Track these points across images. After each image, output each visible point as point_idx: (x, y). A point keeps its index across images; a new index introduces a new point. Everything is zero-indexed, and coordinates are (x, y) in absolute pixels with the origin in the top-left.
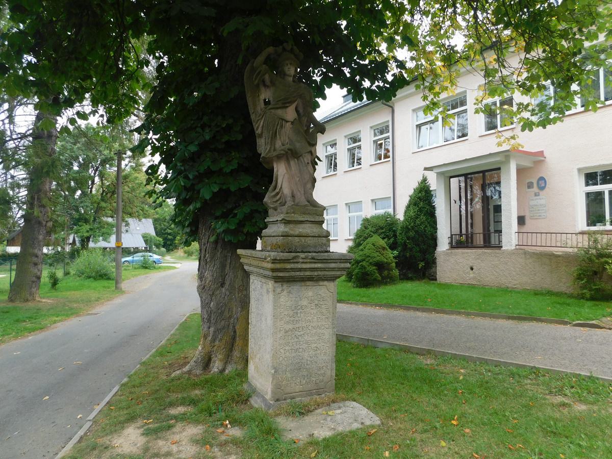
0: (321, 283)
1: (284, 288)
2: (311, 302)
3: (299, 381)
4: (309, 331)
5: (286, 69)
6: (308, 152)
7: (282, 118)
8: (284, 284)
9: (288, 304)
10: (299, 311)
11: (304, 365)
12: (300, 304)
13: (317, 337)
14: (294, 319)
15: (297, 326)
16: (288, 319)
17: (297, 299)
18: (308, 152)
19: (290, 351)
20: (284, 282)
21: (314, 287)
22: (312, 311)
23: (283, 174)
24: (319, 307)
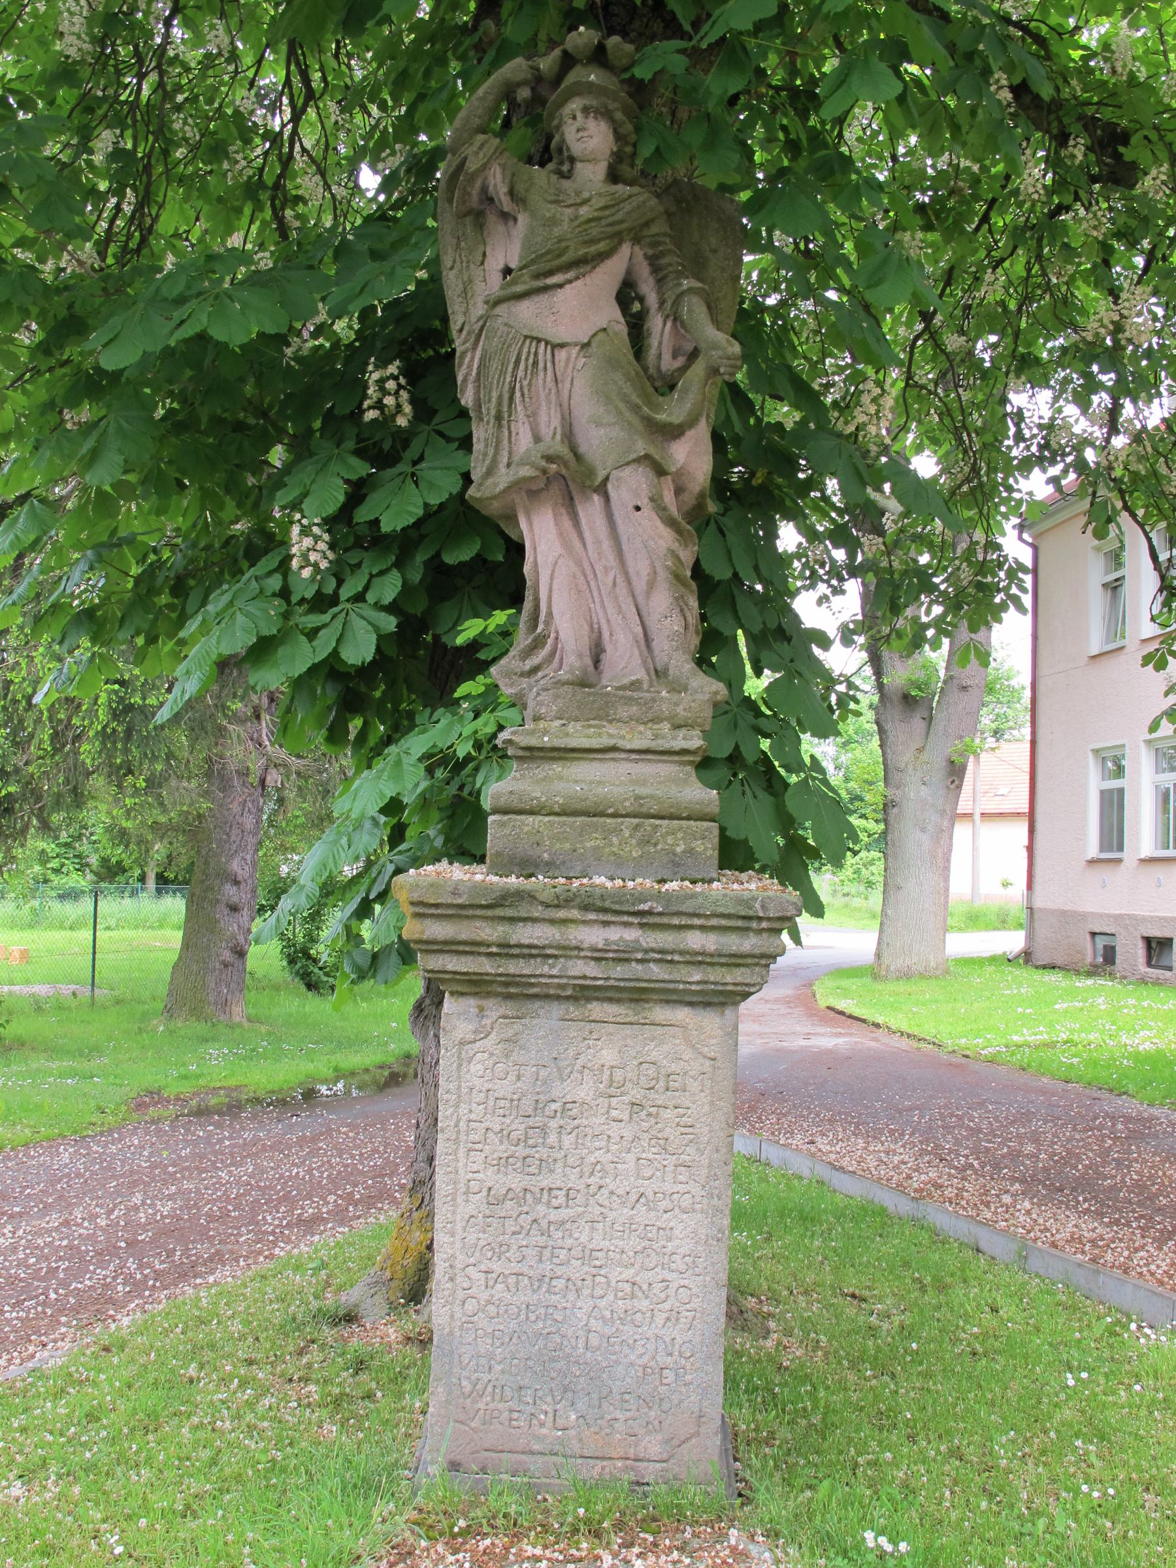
0: (661, 1013)
1: (487, 1022)
2: (613, 1089)
3: (550, 1409)
4: (597, 1210)
5: (570, 133)
6: (638, 460)
7: (534, 334)
8: (490, 1003)
9: (504, 1088)
10: (553, 1124)
11: (575, 1348)
12: (556, 1093)
13: (634, 1243)
14: (528, 1151)
15: (545, 1183)
16: (502, 1149)
17: (543, 1073)
18: (638, 460)
19: (512, 1280)
20: (488, 995)
21: (628, 1030)
22: (615, 1130)
23: (551, 559)
24: (649, 1115)
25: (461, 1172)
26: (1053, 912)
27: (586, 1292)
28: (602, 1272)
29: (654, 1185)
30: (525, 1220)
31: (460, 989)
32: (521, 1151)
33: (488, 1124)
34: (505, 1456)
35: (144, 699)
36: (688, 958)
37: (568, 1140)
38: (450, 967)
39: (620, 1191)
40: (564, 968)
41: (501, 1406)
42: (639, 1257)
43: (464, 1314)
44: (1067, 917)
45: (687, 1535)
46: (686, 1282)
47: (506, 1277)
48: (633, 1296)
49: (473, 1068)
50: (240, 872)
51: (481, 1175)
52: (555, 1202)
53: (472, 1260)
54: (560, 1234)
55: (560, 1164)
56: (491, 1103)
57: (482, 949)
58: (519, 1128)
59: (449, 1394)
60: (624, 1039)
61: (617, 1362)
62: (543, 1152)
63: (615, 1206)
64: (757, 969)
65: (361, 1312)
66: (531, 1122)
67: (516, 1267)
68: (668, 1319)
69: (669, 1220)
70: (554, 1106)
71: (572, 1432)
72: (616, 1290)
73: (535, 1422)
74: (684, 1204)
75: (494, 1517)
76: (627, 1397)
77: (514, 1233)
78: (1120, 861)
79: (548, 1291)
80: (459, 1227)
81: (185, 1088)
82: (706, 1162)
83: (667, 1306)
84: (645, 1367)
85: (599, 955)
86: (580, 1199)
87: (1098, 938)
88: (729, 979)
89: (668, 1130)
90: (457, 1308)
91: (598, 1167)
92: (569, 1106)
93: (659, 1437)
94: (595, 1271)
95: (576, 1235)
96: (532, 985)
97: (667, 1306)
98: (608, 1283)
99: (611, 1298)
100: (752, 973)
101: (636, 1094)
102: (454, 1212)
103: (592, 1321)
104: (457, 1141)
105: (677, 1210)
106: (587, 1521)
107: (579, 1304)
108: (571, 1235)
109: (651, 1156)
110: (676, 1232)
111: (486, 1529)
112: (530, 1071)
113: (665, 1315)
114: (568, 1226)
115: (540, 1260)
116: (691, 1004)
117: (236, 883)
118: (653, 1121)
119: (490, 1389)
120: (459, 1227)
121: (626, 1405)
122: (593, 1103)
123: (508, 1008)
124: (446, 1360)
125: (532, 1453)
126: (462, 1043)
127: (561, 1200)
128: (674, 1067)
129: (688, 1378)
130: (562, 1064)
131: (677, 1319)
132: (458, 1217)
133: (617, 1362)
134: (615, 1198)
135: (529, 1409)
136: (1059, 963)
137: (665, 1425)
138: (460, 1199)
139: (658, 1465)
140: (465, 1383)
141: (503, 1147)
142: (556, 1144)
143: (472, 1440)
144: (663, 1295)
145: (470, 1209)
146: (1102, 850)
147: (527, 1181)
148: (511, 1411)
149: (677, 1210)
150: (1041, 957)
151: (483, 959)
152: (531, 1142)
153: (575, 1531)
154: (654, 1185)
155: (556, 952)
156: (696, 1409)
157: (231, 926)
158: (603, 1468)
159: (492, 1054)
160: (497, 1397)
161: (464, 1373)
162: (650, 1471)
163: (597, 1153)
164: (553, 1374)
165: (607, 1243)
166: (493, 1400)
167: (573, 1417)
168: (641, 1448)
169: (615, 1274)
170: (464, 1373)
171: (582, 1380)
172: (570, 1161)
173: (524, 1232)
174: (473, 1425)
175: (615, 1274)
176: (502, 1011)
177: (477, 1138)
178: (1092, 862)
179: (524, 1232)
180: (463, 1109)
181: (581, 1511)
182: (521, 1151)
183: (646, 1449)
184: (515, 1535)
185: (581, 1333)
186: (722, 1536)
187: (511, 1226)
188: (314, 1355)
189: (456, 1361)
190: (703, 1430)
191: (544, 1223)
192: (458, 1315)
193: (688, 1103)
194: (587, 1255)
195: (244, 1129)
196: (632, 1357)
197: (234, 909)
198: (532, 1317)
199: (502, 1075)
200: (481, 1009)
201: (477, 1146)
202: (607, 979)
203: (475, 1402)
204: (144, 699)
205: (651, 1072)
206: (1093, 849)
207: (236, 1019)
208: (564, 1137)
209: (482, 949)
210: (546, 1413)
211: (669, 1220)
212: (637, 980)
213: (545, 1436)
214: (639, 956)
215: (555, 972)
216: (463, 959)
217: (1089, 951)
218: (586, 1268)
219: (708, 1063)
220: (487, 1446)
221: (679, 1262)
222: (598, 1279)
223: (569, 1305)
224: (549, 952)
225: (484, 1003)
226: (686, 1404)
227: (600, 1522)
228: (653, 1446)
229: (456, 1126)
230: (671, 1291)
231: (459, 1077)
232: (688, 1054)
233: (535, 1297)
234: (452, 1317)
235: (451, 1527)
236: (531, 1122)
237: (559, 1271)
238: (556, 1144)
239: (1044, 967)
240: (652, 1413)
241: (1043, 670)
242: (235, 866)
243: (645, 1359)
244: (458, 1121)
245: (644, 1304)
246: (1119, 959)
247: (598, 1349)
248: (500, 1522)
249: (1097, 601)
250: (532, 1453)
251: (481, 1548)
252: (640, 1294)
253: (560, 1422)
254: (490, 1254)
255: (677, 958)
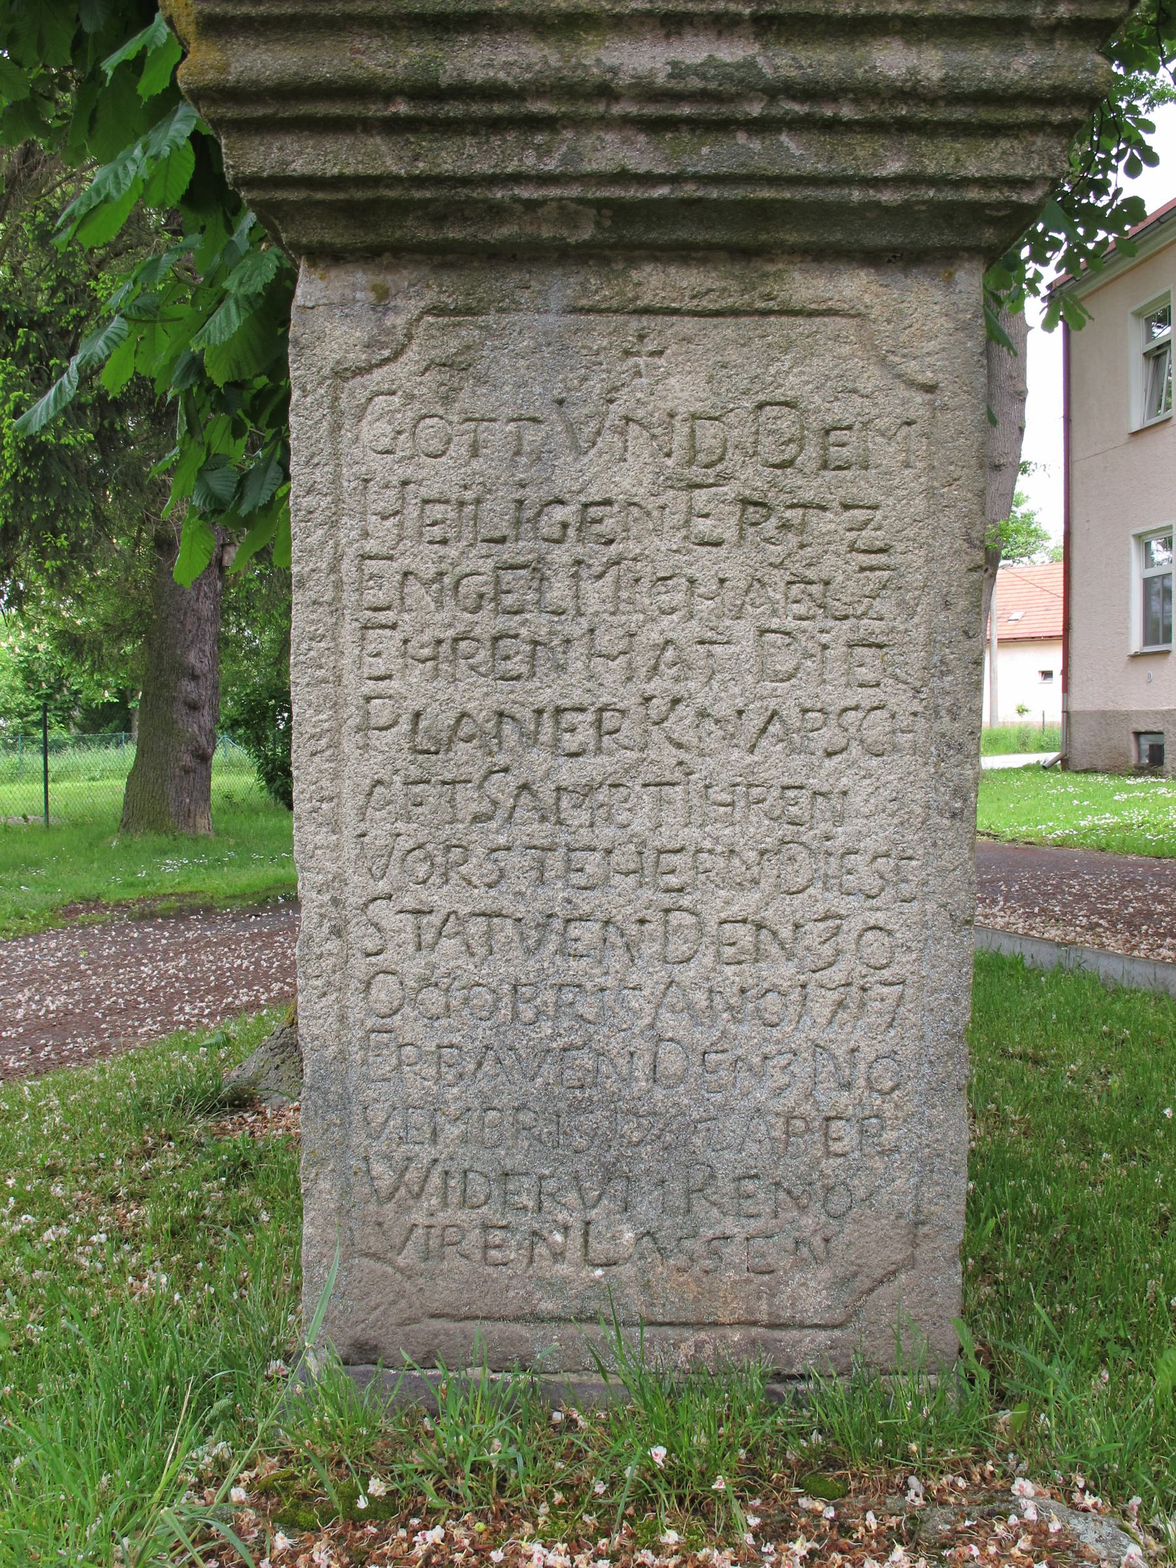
1: (397, 321)
2: (697, 472)
3: (575, 1221)
4: (670, 755)
8: (399, 279)
9: (441, 477)
10: (561, 555)
11: (627, 1080)
12: (563, 483)
13: (758, 829)
15: (546, 697)
16: (445, 620)
17: (532, 436)
21: (728, 328)
22: (705, 565)
24: (785, 526)
25: (349, 679)
26: (1091, 714)
27: (650, 949)
28: (686, 901)
29: (803, 691)
30: (501, 787)
31: (328, 236)
32: (487, 623)
33: (405, 562)
34: (476, 1328)
35: (58, 438)
36: (874, 110)
37: (595, 594)
38: (298, 167)
39: (723, 709)
40: (574, 154)
41: (462, 1216)
42: (770, 868)
43: (370, 1012)
44: (1105, 717)
45: (914, 1497)
46: (880, 918)
47: (462, 921)
48: (758, 955)
49: (367, 431)
50: (198, 665)
51: (394, 685)
52: (570, 742)
53: (383, 886)
54: (585, 817)
55: (579, 649)
56: (412, 512)
57: (374, 110)
58: (480, 564)
59: (346, 1192)
60: (719, 349)
61: (725, 1109)
62: (539, 624)
63: (711, 744)
64: (1039, 142)
65: (260, 1093)
66: (506, 553)
67: (485, 899)
68: (841, 1005)
69: (838, 773)
70: (559, 513)
71: (627, 1271)
72: (719, 943)
73: (541, 1249)
74: (871, 735)
75: (453, 1470)
76: (749, 1186)
77: (476, 819)
78: (1168, 652)
79: (561, 951)
80: (349, 810)
81: (131, 895)
82: (919, 635)
83: (836, 975)
84: (789, 1118)
85: (661, 112)
86: (629, 730)
87: (1143, 739)
88: (972, 169)
89: (830, 560)
90: (354, 1000)
91: (670, 654)
92: (594, 512)
93: (825, 1273)
94: (667, 900)
95: (623, 817)
96: (497, 212)
97: (836, 975)
98: (700, 926)
99: (708, 961)
100: (1028, 154)
101: (751, 478)
102: (336, 776)
103: (665, 1015)
104: (336, 608)
105: (855, 750)
106: (675, 1477)
107: (634, 978)
108: (609, 819)
109: (791, 624)
110: (856, 800)
111: (433, 1500)
112: (500, 433)
113: (835, 996)
114: (601, 796)
115: (541, 881)
116: (873, 259)
117: (194, 677)
118: (793, 539)
119: (435, 1180)
120: (349, 810)
121: (749, 1206)
122: (651, 504)
123: (442, 289)
124: (334, 1117)
125: (537, 1318)
126: (342, 374)
127: (585, 735)
128: (839, 412)
129: (889, 1136)
130: (576, 413)
131: (862, 1005)
132: (347, 787)
133: (725, 1109)
134: (709, 725)
135: (528, 1221)
136: (1100, 765)
137: (838, 1244)
138: (348, 745)
139: (822, 1336)
140: (378, 1168)
141: (444, 616)
142: (569, 604)
143: (401, 1294)
144: (827, 950)
145: (374, 766)
146: (1146, 643)
147: (502, 695)
148: (486, 1227)
149: (855, 750)
150: (1079, 761)
151: (377, 142)
152: (508, 600)
153: (644, 1500)
154: (803, 691)
155: (552, 109)
156: (908, 1208)
157: (192, 727)
158: (699, 1346)
159: (410, 397)
160: (454, 1198)
161: (380, 1146)
162: (805, 1347)
163: (665, 621)
164: (580, 1142)
165: (694, 833)
166: (445, 1204)
167: (629, 1236)
168: (783, 1298)
169: (717, 904)
170: (380, 1146)
171: (645, 1151)
172: (603, 641)
173: (501, 814)
174: (401, 1261)
175: (717, 904)
176: (430, 297)
177: (381, 597)
178: (1136, 656)
179: (501, 814)
180: (349, 528)
181: (659, 1453)
182: (487, 623)
183: (794, 1300)
184: (501, 1514)
185: (640, 1043)
186: (998, 1503)
187: (469, 801)
188: (170, 1156)
189: (357, 1119)
190: (924, 1252)
191: (547, 794)
192: (354, 1015)
193: (873, 495)
194: (651, 861)
195: (189, 930)
196: (761, 1095)
197: (194, 707)
198: (528, 1013)
199: (436, 445)
200: (383, 295)
201: (382, 617)
202: (674, 179)
203: (403, 1209)
204: (58, 438)
205: (787, 423)
206: (1136, 643)
207: (202, 832)
208: (587, 586)
209: (374, 110)
210: (566, 1229)
211: (838, 773)
212: (751, 179)
213: (566, 1281)
214: (755, 110)
215: (551, 165)
216: (330, 144)
217: (1134, 753)
218: (647, 894)
219: (919, 398)
220: (435, 1306)
221: (863, 870)
222: (675, 918)
223: (610, 982)
224: (536, 107)
225: (389, 279)
226: (883, 1197)
227: (706, 1478)
228: (810, 1293)
229: (334, 569)
230: (846, 940)
231: (336, 454)
232: (871, 378)
233: (532, 963)
234: (342, 1019)
235: (350, 1498)
236: (506, 553)
237: (585, 903)
238: (569, 604)
239: (1086, 771)
240: (808, 1221)
241: (1077, 455)
242: (192, 658)
243: (790, 1099)
244: (338, 558)
245: (784, 972)
246: (1168, 758)
247: (682, 1080)
248: (463, 1484)
249: (1137, 373)
250: (537, 1318)
251: (419, 1551)
252: (774, 950)
253: (599, 1248)
254: (422, 870)
255: (847, 112)
